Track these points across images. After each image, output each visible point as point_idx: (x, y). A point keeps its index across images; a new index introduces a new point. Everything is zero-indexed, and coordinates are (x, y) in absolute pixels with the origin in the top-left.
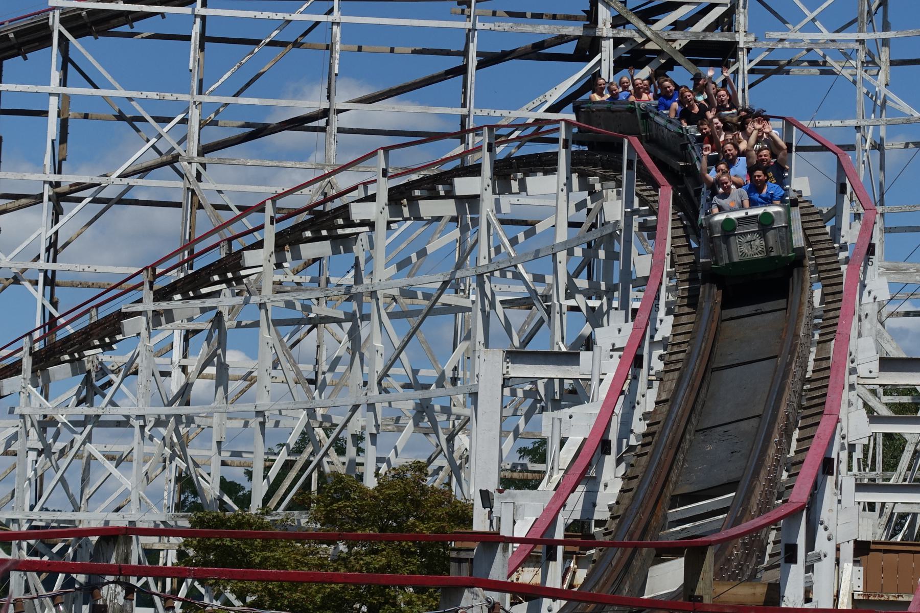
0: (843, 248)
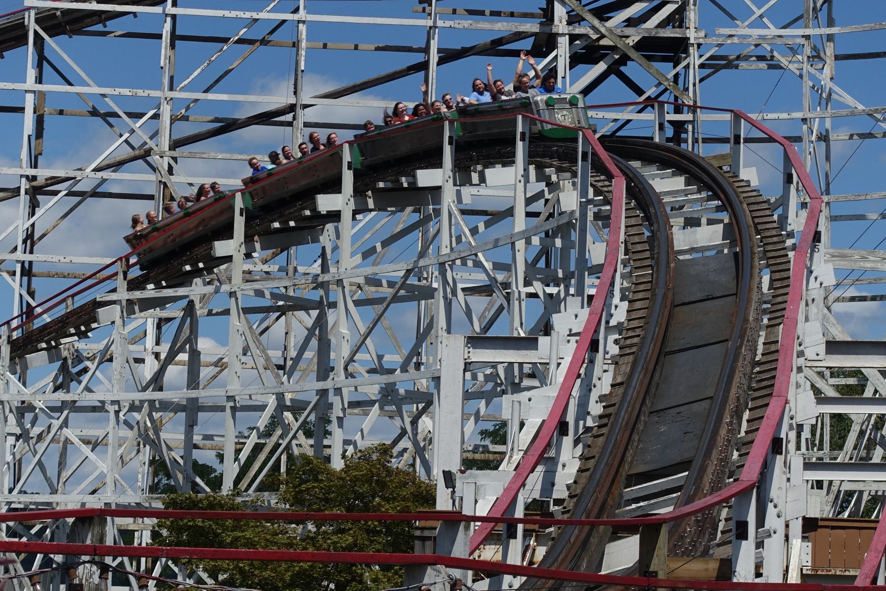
0: (790, 235)
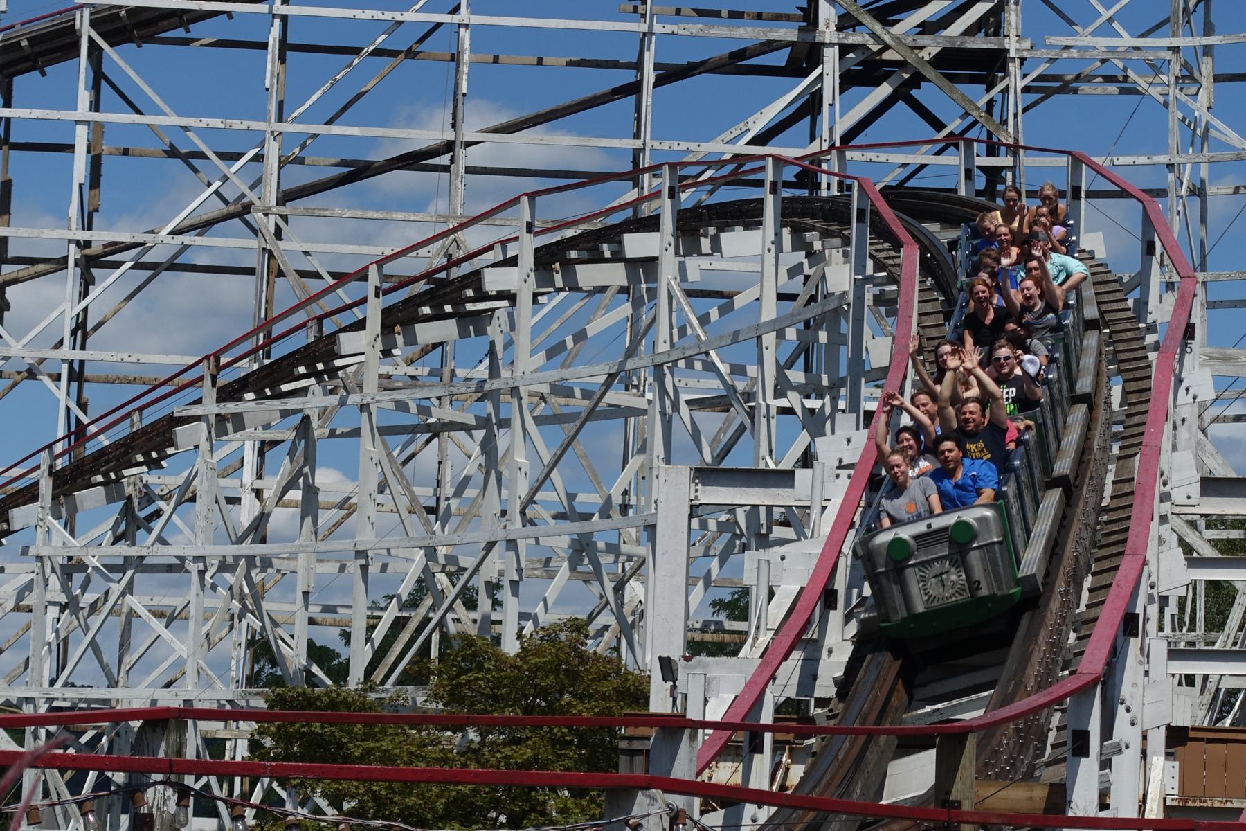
0: (1152, 328)
